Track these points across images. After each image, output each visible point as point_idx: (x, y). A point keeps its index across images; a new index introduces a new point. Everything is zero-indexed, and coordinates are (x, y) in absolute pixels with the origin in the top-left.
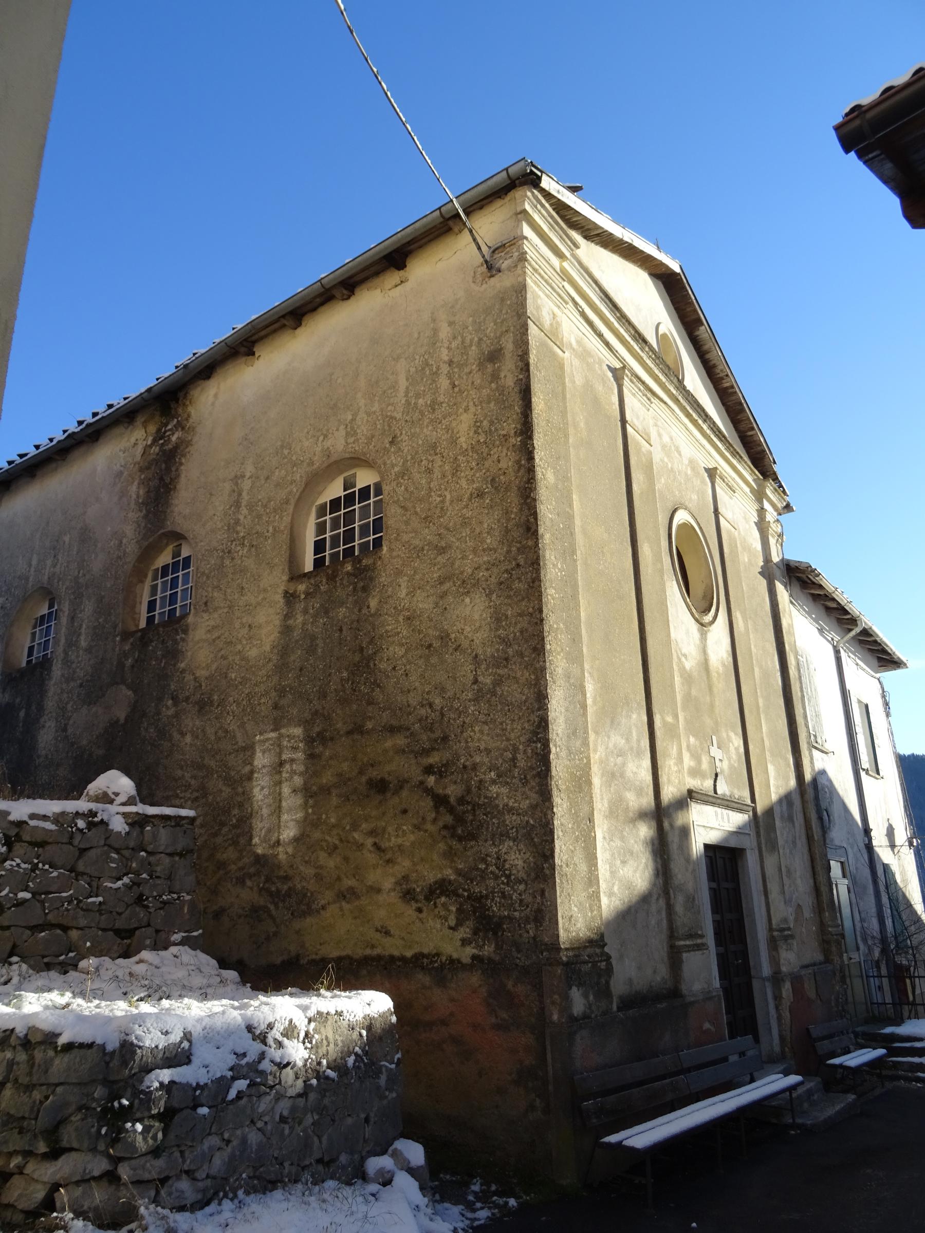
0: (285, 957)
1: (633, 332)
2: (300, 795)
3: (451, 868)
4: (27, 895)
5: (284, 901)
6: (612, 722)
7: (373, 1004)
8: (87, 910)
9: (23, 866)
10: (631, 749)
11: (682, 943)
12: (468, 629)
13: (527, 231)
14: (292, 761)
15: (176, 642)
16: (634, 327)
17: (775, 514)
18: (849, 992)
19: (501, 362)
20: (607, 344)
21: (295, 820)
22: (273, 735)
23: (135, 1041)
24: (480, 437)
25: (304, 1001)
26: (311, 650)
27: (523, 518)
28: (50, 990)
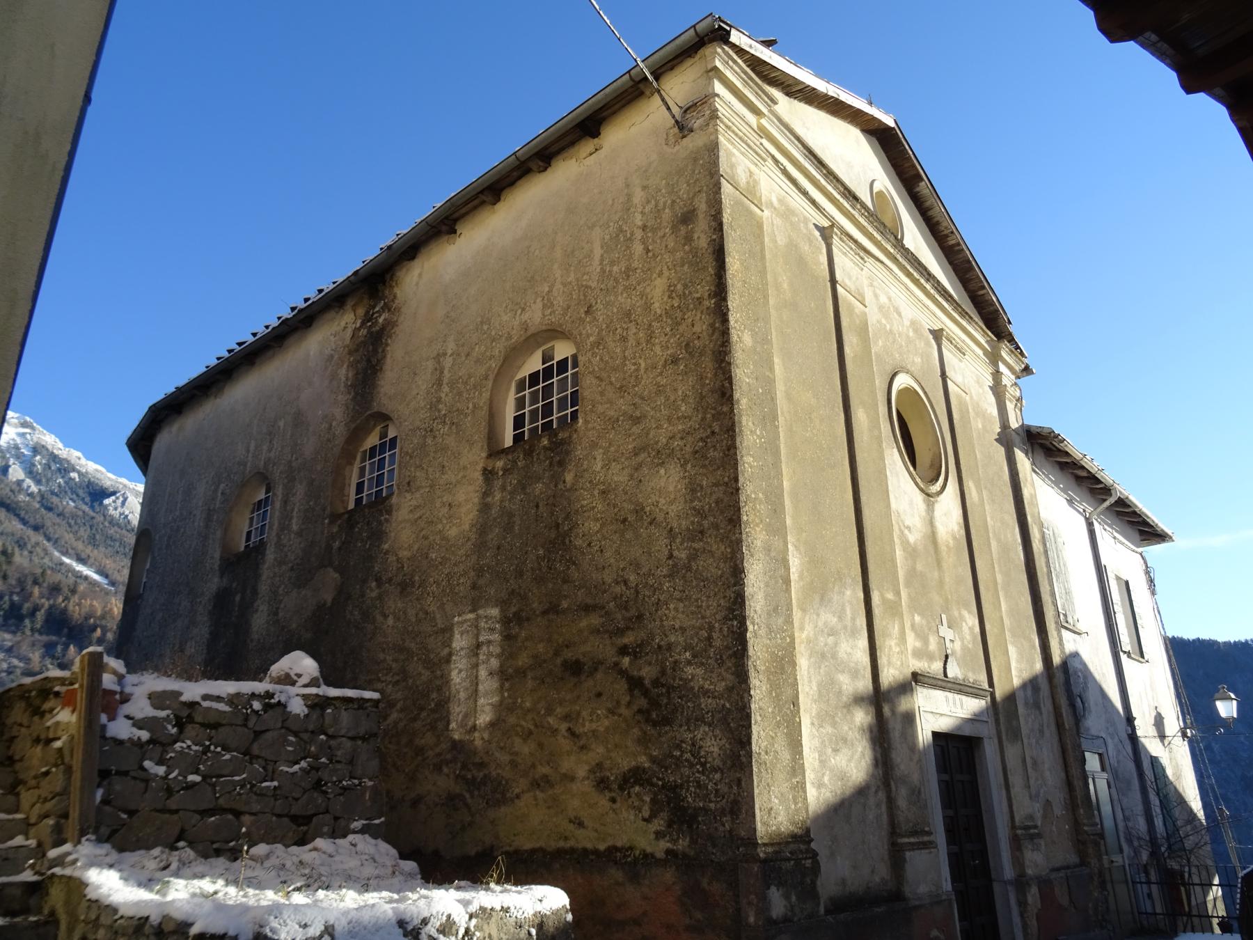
0: (480, 848)
2: (496, 678)
4: (197, 778)
5: (479, 789)
6: (822, 599)
7: (550, 899)
8: (262, 794)
9: (194, 748)
11: (906, 840)
12: (662, 501)
13: (719, 88)
14: (489, 642)
15: (380, 523)
16: (843, 184)
17: (1013, 377)
18: (1111, 899)
20: (813, 202)
21: (491, 704)
22: (471, 616)
23: (269, 934)
25: (466, 895)
26: (508, 528)
28: (202, 877)
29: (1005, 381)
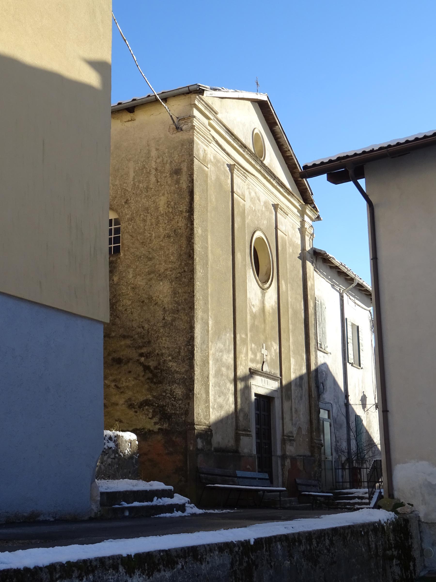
1: (240, 144)
3: (150, 395)
6: (218, 338)
10: (226, 349)
11: (241, 432)
12: (161, 296)
19: (180, 175)
20: (228, 154)
24: (170, 209)
27: (188, 251)
29: (307, 226)
